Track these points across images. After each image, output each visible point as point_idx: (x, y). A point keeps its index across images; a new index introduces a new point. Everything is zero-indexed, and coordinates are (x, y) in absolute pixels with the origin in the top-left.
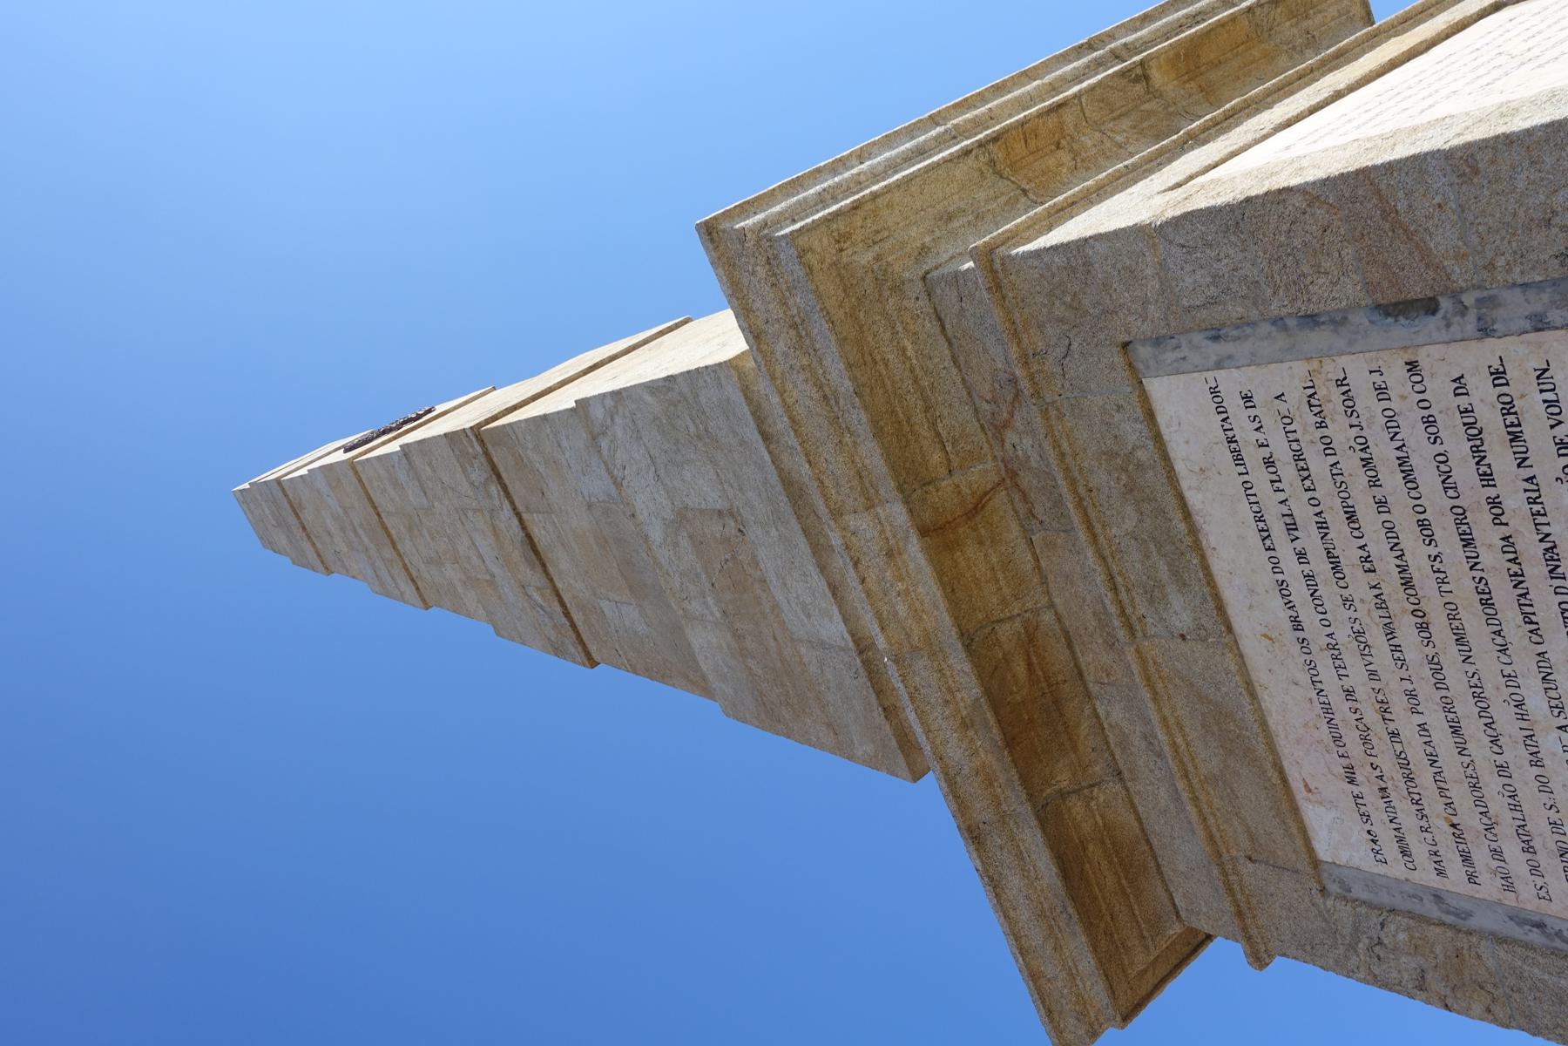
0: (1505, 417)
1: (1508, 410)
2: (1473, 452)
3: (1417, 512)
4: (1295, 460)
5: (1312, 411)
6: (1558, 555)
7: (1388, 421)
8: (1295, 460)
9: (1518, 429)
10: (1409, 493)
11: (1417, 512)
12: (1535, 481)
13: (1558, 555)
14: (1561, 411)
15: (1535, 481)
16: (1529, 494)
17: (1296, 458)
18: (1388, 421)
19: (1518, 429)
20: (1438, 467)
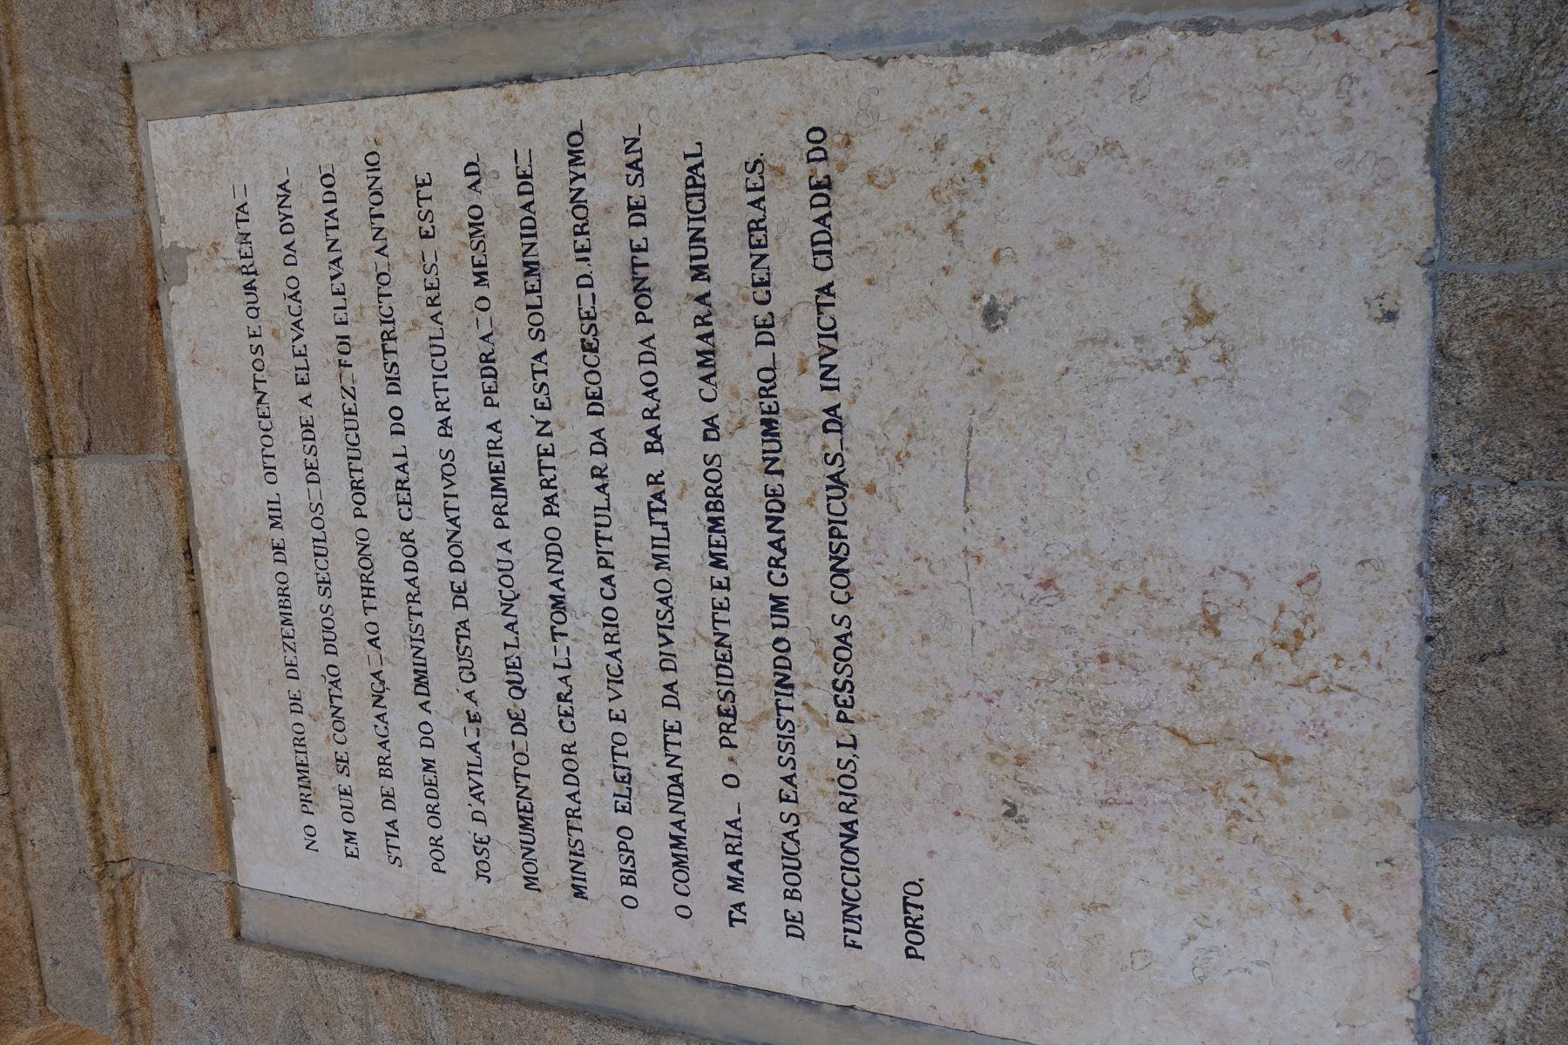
0: (716, 611)
1: (715, 491)
2: (490, 448)
3: (686, 907)
4: (568, 816)
5: (447, 516)
6: (703, 177)
7: (550, 545)
8: (568, 816)
9: (722, 550)
10: (675, 885)
11: (686, 907)
12: (675, 688)
13: (703, 177)
14: (781, 448)
15: (743, 908)
16: (729, 840)
17: (296, 742)
18: (550, 545)
19: (722, 550)
20: (844, 890)
